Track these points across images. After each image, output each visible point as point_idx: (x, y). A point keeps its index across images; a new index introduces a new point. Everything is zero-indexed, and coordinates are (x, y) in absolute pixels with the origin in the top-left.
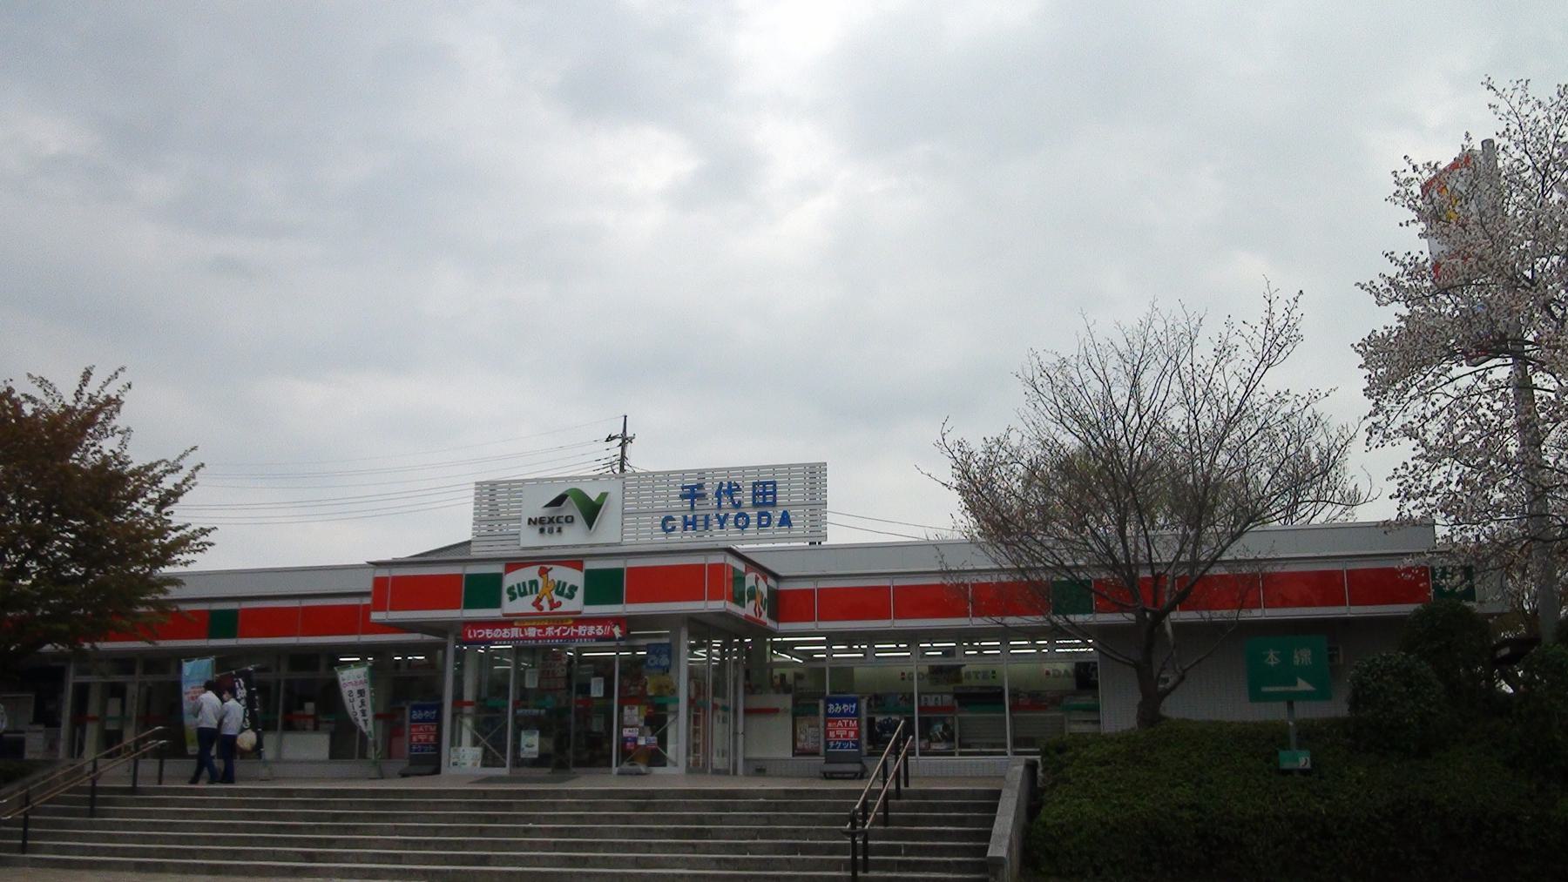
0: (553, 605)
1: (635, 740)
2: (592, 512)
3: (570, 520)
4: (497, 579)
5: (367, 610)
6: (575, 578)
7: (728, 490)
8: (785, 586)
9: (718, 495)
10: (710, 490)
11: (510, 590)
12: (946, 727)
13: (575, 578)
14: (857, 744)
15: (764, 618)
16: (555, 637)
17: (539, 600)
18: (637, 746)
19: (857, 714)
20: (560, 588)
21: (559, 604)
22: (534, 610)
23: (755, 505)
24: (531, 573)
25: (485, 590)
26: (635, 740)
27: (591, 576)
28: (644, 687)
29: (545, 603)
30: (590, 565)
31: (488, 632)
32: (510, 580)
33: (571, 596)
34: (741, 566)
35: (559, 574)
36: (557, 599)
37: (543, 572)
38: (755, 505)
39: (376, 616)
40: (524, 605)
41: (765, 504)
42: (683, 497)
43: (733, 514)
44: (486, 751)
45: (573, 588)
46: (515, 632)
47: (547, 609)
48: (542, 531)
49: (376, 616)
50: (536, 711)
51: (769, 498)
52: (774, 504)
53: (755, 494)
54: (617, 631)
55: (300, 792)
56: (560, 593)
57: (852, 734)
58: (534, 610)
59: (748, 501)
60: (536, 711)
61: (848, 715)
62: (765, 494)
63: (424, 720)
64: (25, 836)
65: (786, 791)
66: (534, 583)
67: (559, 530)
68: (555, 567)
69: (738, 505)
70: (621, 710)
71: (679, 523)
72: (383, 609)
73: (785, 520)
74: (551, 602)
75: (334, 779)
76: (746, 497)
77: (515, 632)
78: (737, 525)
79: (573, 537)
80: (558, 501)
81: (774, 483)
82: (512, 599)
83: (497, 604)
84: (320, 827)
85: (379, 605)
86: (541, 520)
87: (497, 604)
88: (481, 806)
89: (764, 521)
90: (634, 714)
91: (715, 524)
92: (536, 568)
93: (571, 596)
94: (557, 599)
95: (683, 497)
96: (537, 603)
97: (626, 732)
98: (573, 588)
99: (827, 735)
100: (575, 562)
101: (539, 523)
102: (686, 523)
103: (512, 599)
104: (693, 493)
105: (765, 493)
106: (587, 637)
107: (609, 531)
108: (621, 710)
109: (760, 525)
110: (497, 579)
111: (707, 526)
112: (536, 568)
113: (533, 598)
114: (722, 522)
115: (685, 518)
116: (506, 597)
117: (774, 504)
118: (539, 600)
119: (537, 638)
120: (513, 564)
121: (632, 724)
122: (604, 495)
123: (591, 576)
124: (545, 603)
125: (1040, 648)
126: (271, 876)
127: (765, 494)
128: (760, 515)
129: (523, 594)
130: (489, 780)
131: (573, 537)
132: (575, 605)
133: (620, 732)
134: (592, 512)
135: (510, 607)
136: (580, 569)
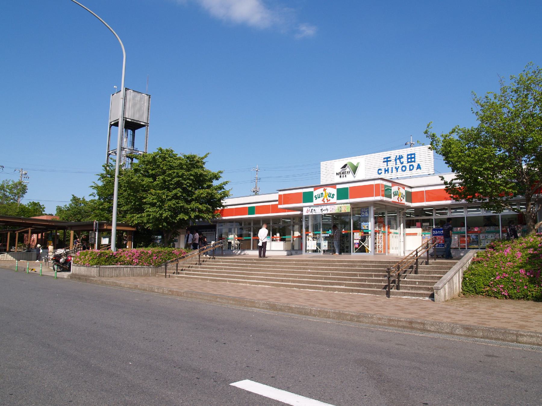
0: (328, 200)
3: (348, 172)
5: (277, 205)
6: (334, 191)
8: (413, 190)
9: (396, 160)
13: (334, 191)
15: (404, 201)
17: (324, 199)
20: (329, 195)
22: (322, 202)
24: (321, 190)
27: (339, 190)
29: (325, 200)
30: (338, 187)
32: (316, 193)
34: (390, 184)
36: (329, 198)
37: (325, 190)
38: (408, 162)
39: (280, 206)
40: (319, 201)
41: (411, 162)
43: (401, 166)
45: (333, 195)
48: (340, 177)
49: (280, 206)
52: (414, 161)
53: (408, 159)
55: (293, 260)
58: (322, 202)
66: (322, 194)
68: (328, 188)
70: (353, 234)
71: (383, 171)
72: (281, 204)
73: (419, 167)
76: (405, 160)
79: (350, 177)
81: (408, 155)
83: (312, 201)
85: (280, 204)
87: (312, 201)
91: (394, 170)
92: (323, 189)
94: (329, 198)
96: (323, 200)
98: (333, 195)
102: (385, 171)
113: (322, 198)
116: (314, 198)
117: (414, 161)
118: (324, 199)
122: (358, 163)
123: (339, 190)
124: (325, 200)
127: (411, 158)
130: (314, 257)
131: (350, 177)
133: (110, 241)
135: (316, 202)
136: (335, 188)
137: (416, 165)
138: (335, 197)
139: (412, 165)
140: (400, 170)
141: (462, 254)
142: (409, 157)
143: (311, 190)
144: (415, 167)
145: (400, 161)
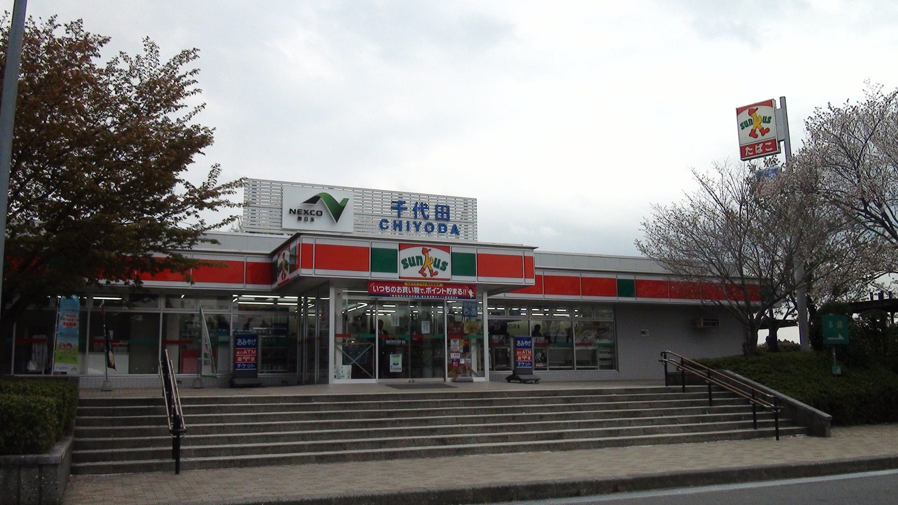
1: (458, 360)
2: (337, 210)
3: (319, 214)
4: (394, 253)
6: (446, 257)
7: (421, 208)
9: (415, 210)
10: (410, 205)
11: (404, 261)
12: (543, 354)
13: (446, 257)
14: (256, 365)
16: (432, 294)
18: (459, 365)
19: (256, 346)
21: (436, 273)
22: (420, 276)
23: (437, 219)
24: (416, 252)
25: (385, 259)
26: (458, 360)
28: (462, 328)
29: (427, 272)
30: (455, 250)
31: (387, 288)
32: (404, 255)
33: (444, 269)
35: (435, 253)
36: (435, 270)
37: (425, 252)
38: (437, 219)
40: (413, 272)
42: (392, 208)
43: (424, 223)
44: (354, 367)
45: (445, 264)
46: (405, 289)
47: (428, 276)
48: (300, 219)
50: (399, 342)
51: (445, 216)
52: (448, 219)
53: (437, 212)
54: (471, 293)
56: (437, 266)
57: (253, 359)
59: (432, 215)
60: (399, 342)
61: (251, 346)
62: (442, 213)
63: (247, 346)
64: (755, 417)
65: (625, 390)
67: (312, 220)
69: (426, 218)
71: (390, 224)
73: (455, 230)
74: (431, 271)
75: (570, 382)
76: (431, 213)
77: (405, 289)
78: (426, 230)
79: (322, 225)
80: (314, 200)
81: (448, 207)
82: (405, 268)
84: (401, 421)
86: (299, 212)
88: (473, 403)
89: (442, 229)
90: (457, 345)
91: (413, 228)
92: (421, 248)
93: (444, 269)
94: (435, 270)
95: (392, 208)
97: (453, 356)
98: (445, 264)
99: (235, 359)
100: (445, 247)
101: (298, 214)
103: (405, 268)
104: (399, 206)
105: (443, 212)
106: (452, 295)
107: (347, 224)
108: (449, 342)
109: (440, 231)
110: (394, 253)
111: (408, 229)
112: (421, 248)
113: (420, 267)
114: (417, 227)
115: (395, 222)
116: (400, 266)
119: (420, 295)
120: (404, 245)
121: (453, 350)
122: (345, 201)
124: (427, 272)
125: (545, 313)
126: (251, 466)
127: (442, 213)
128: (440, 226)
129: (413, 265)
131: (322, 225)
132: (445, 274)
133: (449, 356)
134: (337, 210)
137: (450, 226)
138: (449, 268)
139: (444, 225)
140: (422, 227)
141: (140, 319)
142: (445, 210)
143: (395, 246)
144: (449, 228)
145: (423, 214)
